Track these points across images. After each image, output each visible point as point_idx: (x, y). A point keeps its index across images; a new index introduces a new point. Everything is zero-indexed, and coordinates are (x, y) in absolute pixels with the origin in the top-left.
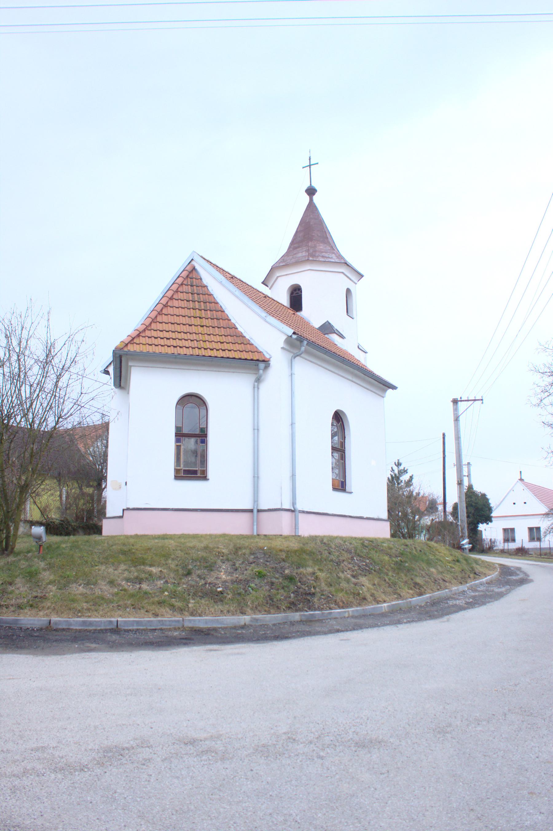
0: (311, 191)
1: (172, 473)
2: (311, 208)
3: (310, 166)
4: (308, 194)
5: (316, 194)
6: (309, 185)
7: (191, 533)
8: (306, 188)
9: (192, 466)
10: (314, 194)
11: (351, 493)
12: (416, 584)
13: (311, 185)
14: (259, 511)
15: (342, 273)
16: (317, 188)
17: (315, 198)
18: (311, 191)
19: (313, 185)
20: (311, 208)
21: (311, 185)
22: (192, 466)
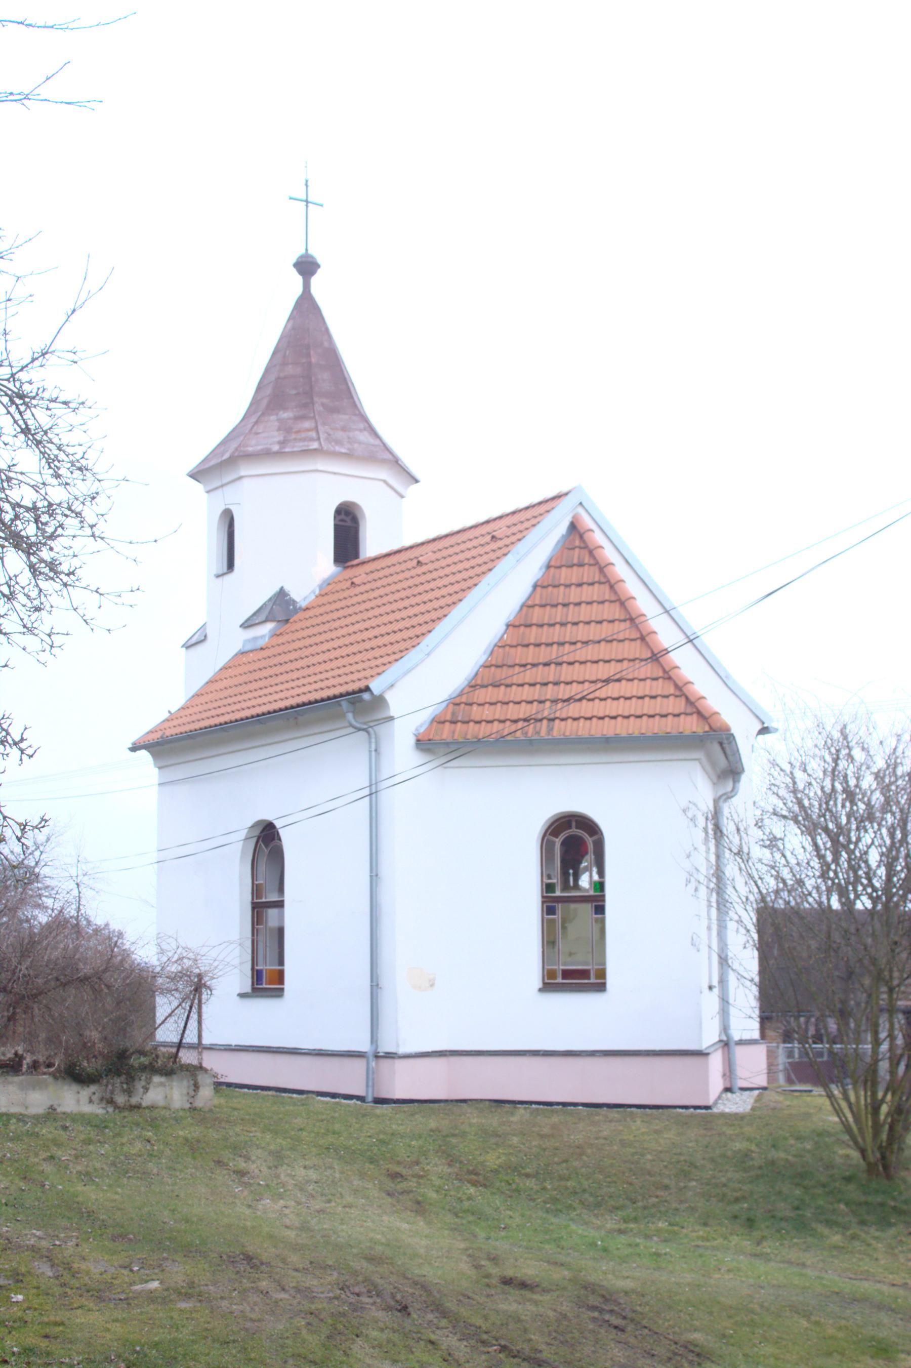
0: (307, 267)
1: (535, 978)
2: (306, 308)
3: (307, 202)
4: (301, 272)
5: (319, 271)
6: (303, 252)
7: (430, 1050)
8: (294, 260)
9: (573, 843)
10: (313, 273)
11: (134, 748)
12: (151, 1265)
13: (307, 250)
14: (377, 1057)
15: (385, 482)
16: (319, 261)
17: (316, 281)
18: (307, 267)
19: (310, 252)
20: (306, 308)
21: (307, 250)
22: (573, 843)
